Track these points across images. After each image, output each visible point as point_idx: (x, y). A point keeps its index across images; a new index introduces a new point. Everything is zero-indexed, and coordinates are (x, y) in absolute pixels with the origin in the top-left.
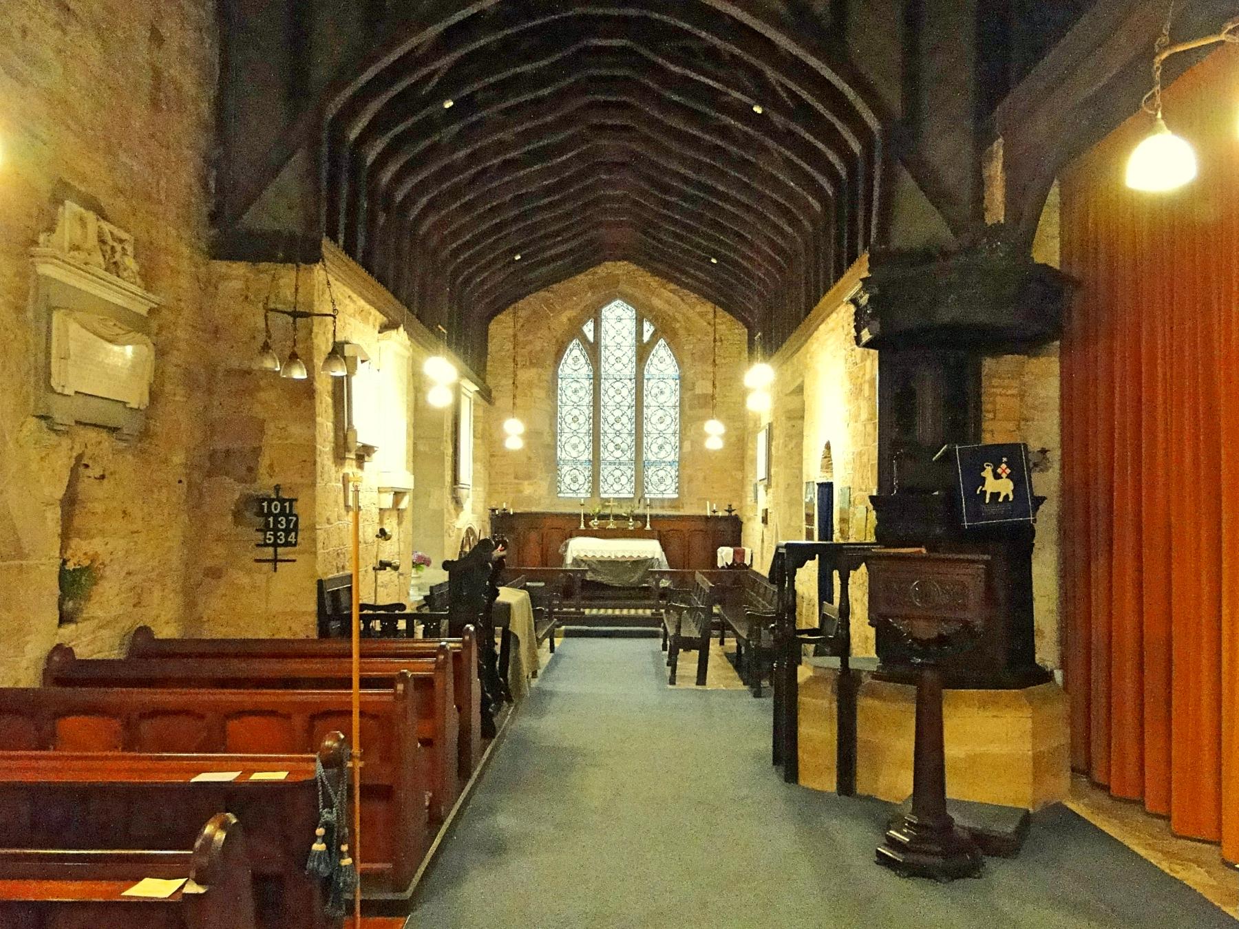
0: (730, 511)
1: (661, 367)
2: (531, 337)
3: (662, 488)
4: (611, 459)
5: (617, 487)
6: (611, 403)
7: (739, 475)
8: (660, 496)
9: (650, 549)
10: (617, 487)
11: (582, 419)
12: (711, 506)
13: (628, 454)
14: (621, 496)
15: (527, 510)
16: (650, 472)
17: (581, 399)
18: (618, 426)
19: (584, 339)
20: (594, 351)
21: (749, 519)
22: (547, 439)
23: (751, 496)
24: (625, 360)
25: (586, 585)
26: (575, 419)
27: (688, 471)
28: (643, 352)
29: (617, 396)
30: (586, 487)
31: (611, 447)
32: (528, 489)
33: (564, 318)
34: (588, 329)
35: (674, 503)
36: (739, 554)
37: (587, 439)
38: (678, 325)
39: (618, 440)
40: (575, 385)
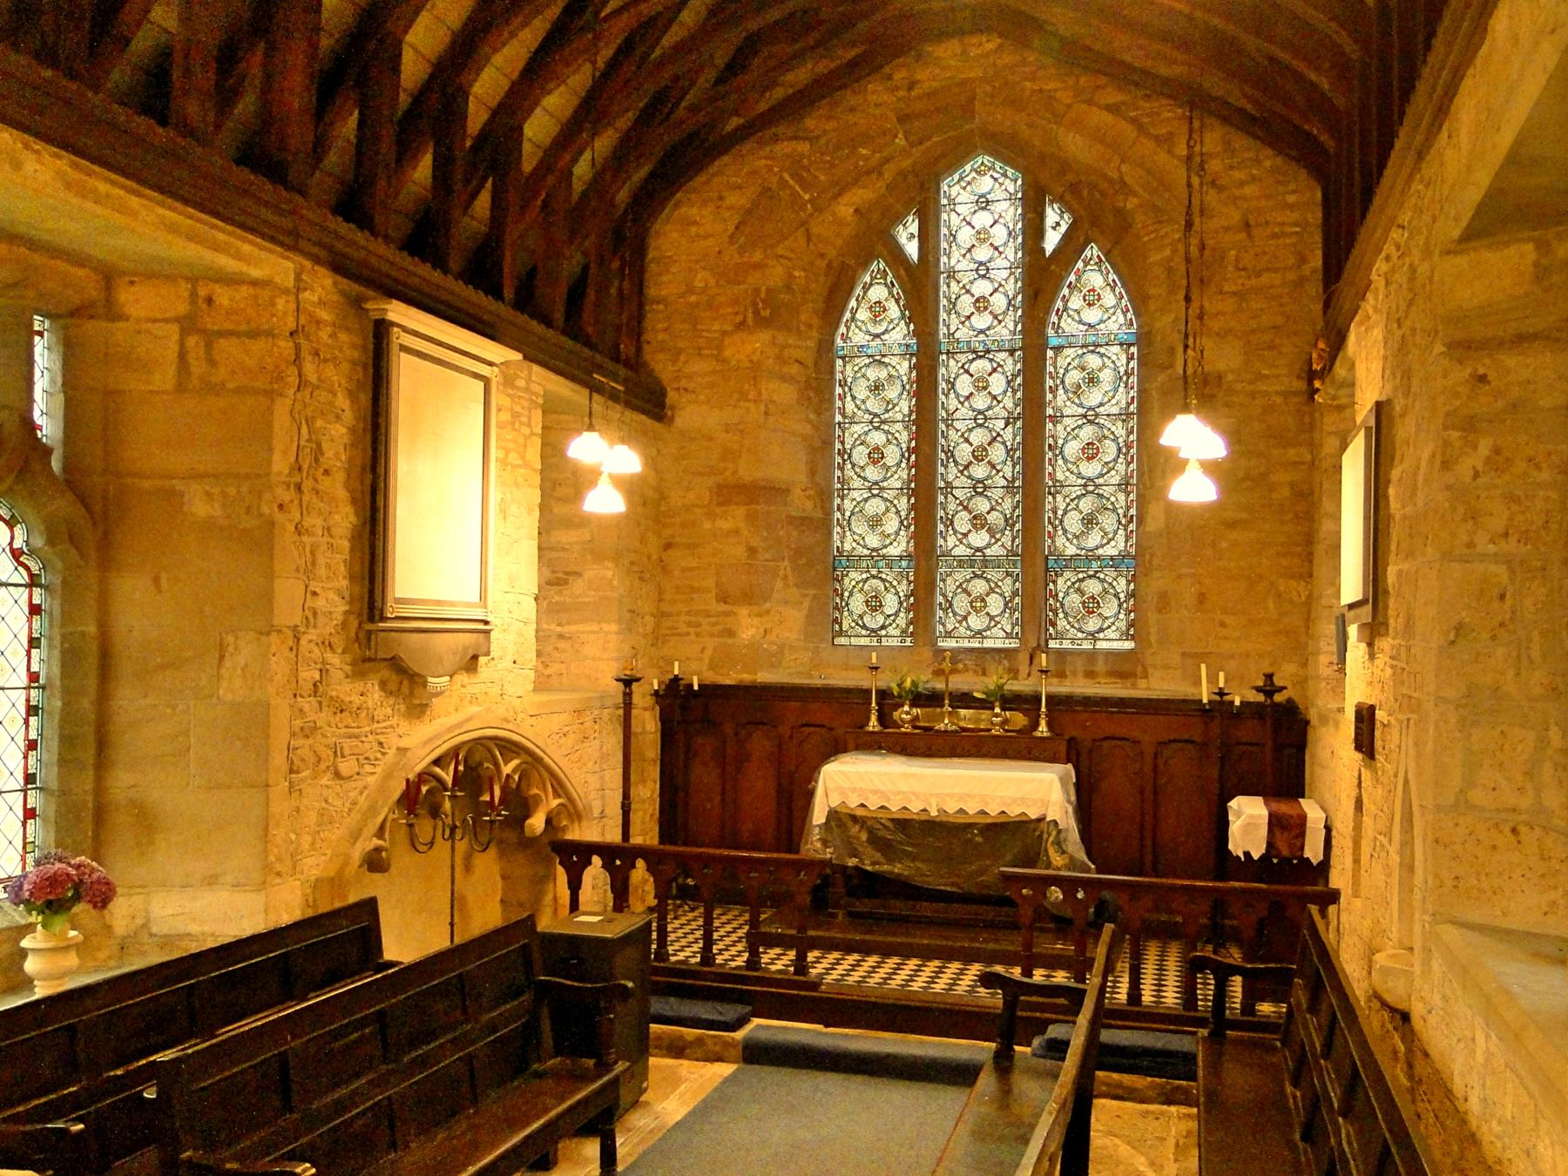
0: (1269, 689)
1: (1092, 315)
2: (758, 256)
3: (1092, 624)
4: (961, 551)
5: (976, 622)
6: (964, 412)
7: (1297, 589)
8: (1087, 645)
9: (1038, 791)
10: (979, 618)
11: (892, 455)
12: (1212, 679)
13: (1006, 540)
14: (988, 644)
15: (746, 678)
16: (951, 585)
17: (890, 405)
18: (979, 471)
19: (896, 256)
20: (920, 288)
21: (1324, 719)
22: (801, 503)
23: (1328, 647)
24: (999, 302)
25: (868, 884)
26: (876, 456)
27: (1158, 582)
28: (1041, 281)
29: (979, 394)
30: (902, 620)
31: (962, 522)
32: (748, 627)
33: (845, 209)
34: (908, 238)
35: (1122, 666)
36: (1286, 827)
37: (903, 504)
38: (1132, 203)
39: (982, 505)
40: (874, 373)
